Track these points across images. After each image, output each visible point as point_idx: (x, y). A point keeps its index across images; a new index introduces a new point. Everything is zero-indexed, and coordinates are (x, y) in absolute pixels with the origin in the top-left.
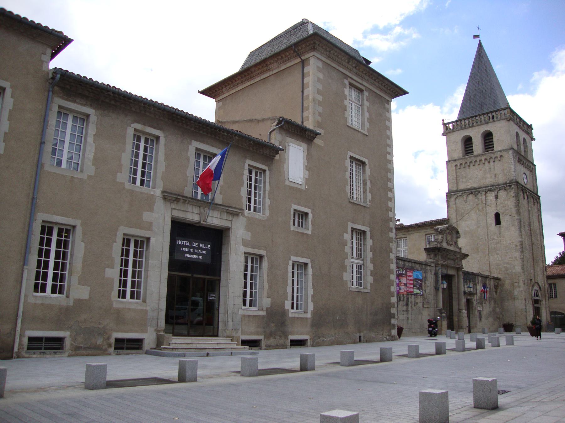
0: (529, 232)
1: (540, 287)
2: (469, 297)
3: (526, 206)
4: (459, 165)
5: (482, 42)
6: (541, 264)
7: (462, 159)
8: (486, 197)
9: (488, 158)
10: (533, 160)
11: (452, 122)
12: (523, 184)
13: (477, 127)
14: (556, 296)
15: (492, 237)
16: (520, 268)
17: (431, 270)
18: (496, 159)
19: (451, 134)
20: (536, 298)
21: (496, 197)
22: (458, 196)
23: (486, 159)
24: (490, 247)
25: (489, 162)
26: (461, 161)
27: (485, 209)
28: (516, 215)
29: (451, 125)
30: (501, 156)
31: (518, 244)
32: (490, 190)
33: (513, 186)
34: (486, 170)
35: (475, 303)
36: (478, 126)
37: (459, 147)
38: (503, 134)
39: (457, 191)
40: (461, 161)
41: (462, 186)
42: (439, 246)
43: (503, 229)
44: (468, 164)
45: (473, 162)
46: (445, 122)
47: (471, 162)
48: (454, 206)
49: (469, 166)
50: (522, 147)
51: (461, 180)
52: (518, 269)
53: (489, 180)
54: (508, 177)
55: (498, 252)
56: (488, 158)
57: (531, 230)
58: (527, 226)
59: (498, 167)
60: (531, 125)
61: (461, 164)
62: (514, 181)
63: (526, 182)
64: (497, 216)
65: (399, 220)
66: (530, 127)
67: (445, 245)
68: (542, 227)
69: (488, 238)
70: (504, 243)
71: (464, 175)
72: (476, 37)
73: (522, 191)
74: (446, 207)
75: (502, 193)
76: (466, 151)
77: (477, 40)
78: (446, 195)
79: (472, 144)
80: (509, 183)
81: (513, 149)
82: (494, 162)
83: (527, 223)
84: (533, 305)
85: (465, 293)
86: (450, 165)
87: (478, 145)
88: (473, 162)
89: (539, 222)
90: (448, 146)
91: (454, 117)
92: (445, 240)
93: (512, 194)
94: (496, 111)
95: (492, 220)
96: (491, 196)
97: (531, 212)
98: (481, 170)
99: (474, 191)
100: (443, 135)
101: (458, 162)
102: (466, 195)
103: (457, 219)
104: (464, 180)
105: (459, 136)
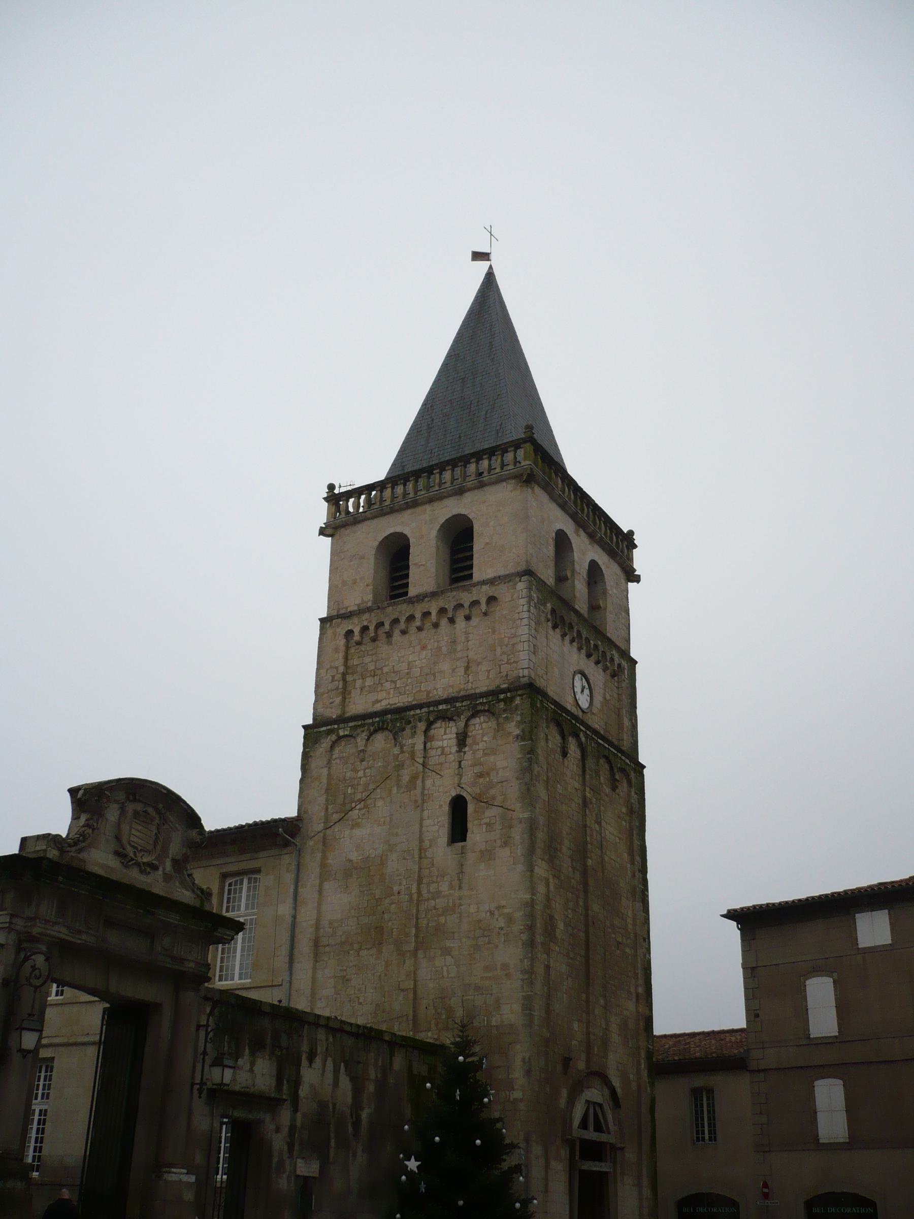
0: (578, 876)
1: (613, 1093)
4: (357, 630)
5: (496, 272)
8: (428, 739)
9: (450, 606)
10: (628, 641)
13: (427, 507)
14: (713, 1138)
15: (433, 888)
16: (517, 1007)
18: (475, 611)
19: (348, 531)
20: (591, 1135)
21: (462, 740)
22: (340, 738)
23: (442, 611)
24: (423, 923)
25: (452, 621)
27: (419, 783)
28: (517, 806)
30: (492, 600)
31: (518, 915)
32: (445, 717)
33: (518, 701)
34: (439, 649)
35: (278, 1142)
36: (430, 501)
37: (367, 572)
38: (509, 527)
39: (342, 720)
40: (370, 620)
41: (359, 704)
43: (471, 857)
44: (387, 626)
45: (403, 619)
47: (396, 621)
48: (325, 771)
49: (389, 635)
51: (359, 683)
52: (511, 1013)
53: (447, 682)
54: (505, 668)
55: (448, 944)
56: (450, 606)
57: (585, 873)
58: (566, 849)
59: (473, 635)
60: (631, 533)
62: (524, 681)
64: (458, 806)
66: (627, 541)
69: (419, 893)
70: (472, 909)
71: (371, 667)
72: (478, 256)
73: (559, 725)
74: (299, 775)
75: (481, 727)
76: (393, 588)
77: (482, 267)
78: (302, 732)
80: (503, 691)
81: (529, 572)
82: (468, 618)
86: (330, 631)
87: (425, 567)
88: (403, 619)
89: (631, 853)
90: (334, 569)
93: (513, 728)
94: (491, 452)
96: (445, 736)
98: (424, 648)
99: (391, 721)
100: (322, 532)
101: (355, 620)
102: (364, 735)
103: (327, 820)
104: (369, 682)
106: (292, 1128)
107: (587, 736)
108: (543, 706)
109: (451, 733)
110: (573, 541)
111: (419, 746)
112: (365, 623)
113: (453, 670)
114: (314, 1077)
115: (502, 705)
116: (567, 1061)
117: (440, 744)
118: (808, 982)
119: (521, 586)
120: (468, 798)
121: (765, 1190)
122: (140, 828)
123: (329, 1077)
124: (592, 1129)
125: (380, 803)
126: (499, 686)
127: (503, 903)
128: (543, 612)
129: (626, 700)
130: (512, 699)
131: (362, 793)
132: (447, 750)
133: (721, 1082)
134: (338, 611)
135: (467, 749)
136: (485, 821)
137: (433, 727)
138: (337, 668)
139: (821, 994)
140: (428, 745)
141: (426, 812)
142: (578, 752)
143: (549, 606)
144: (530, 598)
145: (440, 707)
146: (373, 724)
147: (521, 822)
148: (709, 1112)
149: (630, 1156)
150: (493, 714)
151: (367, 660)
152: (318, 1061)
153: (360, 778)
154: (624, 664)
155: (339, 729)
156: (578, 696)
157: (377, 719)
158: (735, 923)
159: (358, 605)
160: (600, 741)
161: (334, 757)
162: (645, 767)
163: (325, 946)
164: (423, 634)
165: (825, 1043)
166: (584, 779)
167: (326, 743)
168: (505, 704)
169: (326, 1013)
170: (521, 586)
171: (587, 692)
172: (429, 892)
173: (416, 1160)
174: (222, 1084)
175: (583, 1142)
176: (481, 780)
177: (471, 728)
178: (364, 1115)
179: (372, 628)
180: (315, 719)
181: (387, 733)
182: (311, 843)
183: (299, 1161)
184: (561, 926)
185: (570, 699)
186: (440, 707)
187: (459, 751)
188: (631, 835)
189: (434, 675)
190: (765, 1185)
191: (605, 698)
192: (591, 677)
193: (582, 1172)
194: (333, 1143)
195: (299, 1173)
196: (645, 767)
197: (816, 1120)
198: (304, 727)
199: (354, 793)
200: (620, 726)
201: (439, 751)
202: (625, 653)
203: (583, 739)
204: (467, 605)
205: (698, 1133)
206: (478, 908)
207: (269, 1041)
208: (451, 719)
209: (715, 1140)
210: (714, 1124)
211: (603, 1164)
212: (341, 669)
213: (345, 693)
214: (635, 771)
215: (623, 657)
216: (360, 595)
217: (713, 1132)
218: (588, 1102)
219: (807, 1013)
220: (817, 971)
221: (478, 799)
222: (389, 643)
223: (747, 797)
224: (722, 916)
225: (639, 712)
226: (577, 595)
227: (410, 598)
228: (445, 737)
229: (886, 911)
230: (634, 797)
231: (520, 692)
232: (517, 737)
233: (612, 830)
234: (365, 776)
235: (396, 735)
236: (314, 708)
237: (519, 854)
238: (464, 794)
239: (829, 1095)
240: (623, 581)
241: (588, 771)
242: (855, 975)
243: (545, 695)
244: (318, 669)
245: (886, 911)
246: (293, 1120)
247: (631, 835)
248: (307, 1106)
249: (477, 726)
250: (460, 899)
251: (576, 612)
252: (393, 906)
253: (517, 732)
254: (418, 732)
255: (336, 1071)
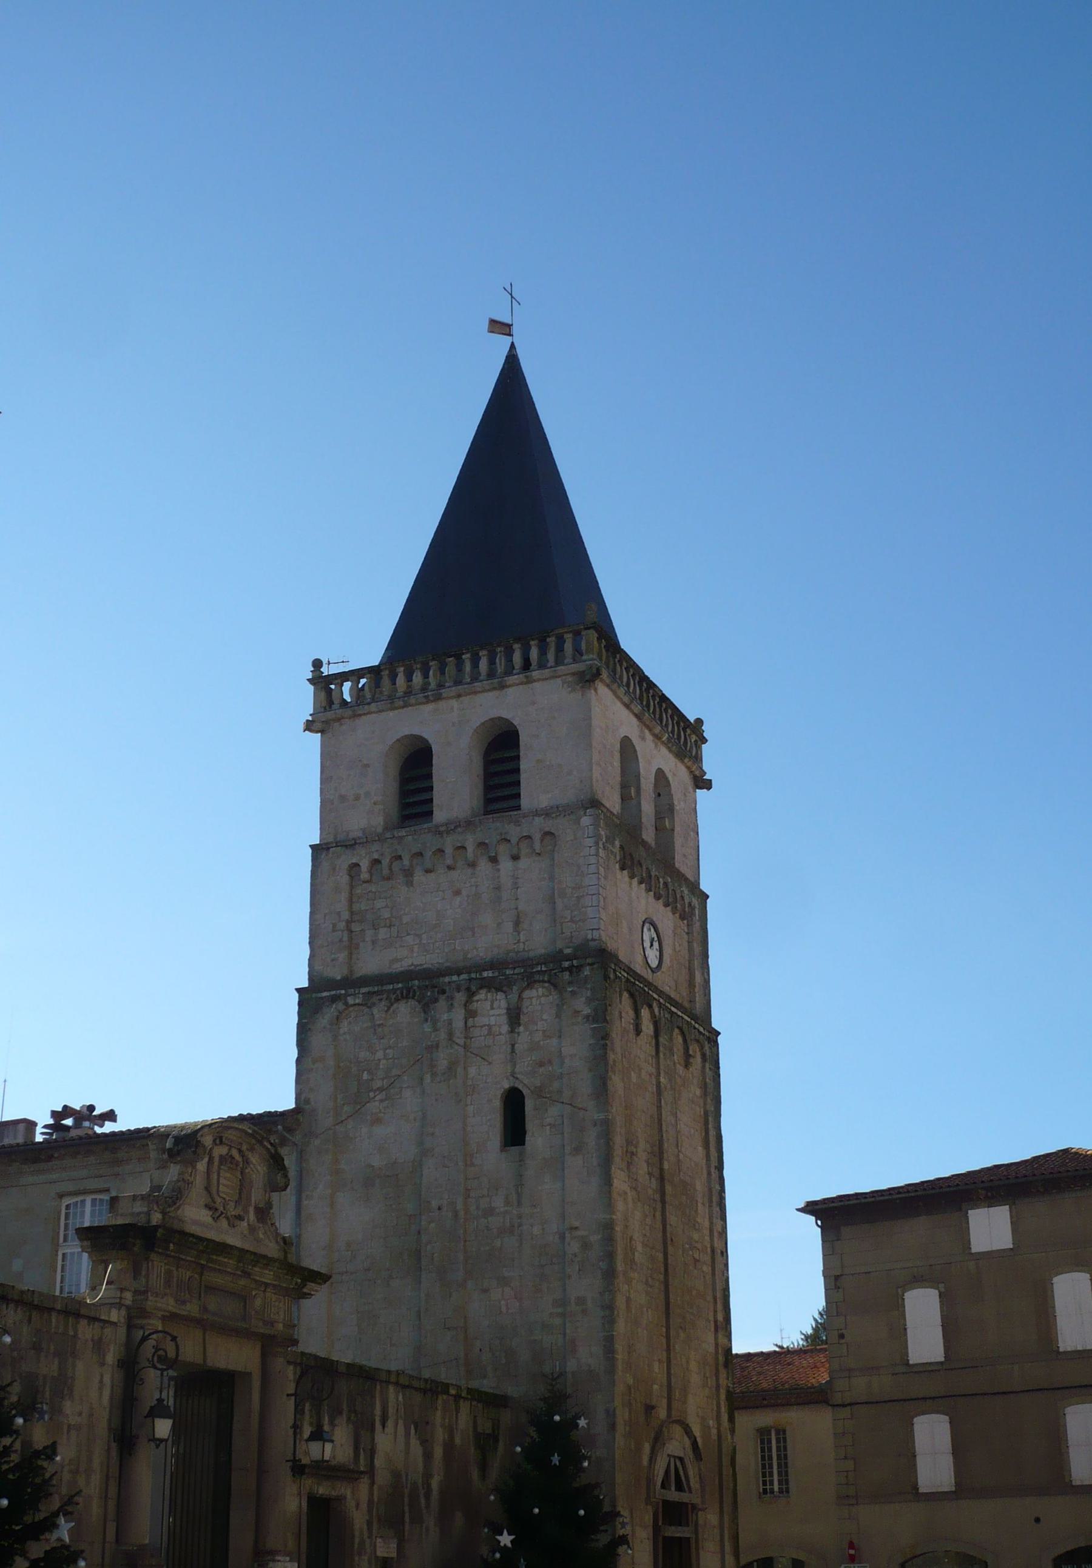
0: (654, 1184)
1: (694, 1443)
2: (322, 1490)
3: (648, 1068)
4: (365, 864)
6: (710, 1337)
7: (380, 839)
11: (354, 675)
12: (639, 968)
14: (785, 1491)
17: (99, 1346)
20: (673, 1495)
21: (514, 1017)
25: (494, 860)
26: (376, 847)
29: (347, 686)
31: (595, 1238)
33: (587, 971)
35: (359, 1519)
37: (378, 788)
38: (567, 733)
39: (350, 983)
41: (371, 963)
42: (156, 1218)
46: (325, 671)
49: (408, 874)
50: (648, 808)
51: (369, 933)
53: (490, 940)
57: (662, 1179)
58: (642, 1155)
60: (699, 722)
61: (377, 862)
63: (654, 963)
64: (514, 1104)
65: (111, 1116)
67: (194, 1216)
68: (720, 1167)
70: (536, 1230)
72: (500, 327)
74: (294, 1053)
75: (538, 1001)
77: (502, 344)
79: (430, 776)
80: (568, 958)
81: (594, 803)
82: (515, 858)
83: (642, 1150)
84: (656, 1530)
85: (298, 1469)
86: (325, 865)
87: (455, 787)
89: (706, 1146)
90: (326, 779)
91: (368, 648)
92: (196, 1193)
93: (582, 1005)
95: (486, 1122)
96: (492, 1009)
97: (667, 1096)
98: (458, 893)
99: (422, 987)
100: (309, 726)
104: (383, 933)
105: (384, 730)
106: (370, 1502)
107: (660, 1005)
108: (616, 977)
109: (499, 1007)
110: (637, 748)
111: (458, 1024)
112: (376, 856)
113: (499, 924)
114: (390, 1443)
115: (566, 976)
116: (649, 1409)
117: (485, 1021)
118: (907, 1295)
119: (586, 821)
120: (525, 1091)
121: (852, 1552)
122: (228, 1175)
123: (401, 1439)
124: (673, 1488)
125: (407, 1093)
126: (561, 951)
127: (577, 1224)
128: (612, 852)
129: (697, 948)
130: (579, 968)
131: (383, 1079)
132: (495, 1029)
133: (793, 1418)
134: (335, 837)
135: (521, 1029)
136: (548, 1120)
137: (476, 998)
138: (339, 913)
139: (923, 1309)
140: (470, 1022)
141: (471, 1109)
142: (651, 1027)
143: (617, 843)
144: (597, 837)
145: (485, 974)
146: (394, 991)
147: (595, 1125)
148: (779, 1456)
149: (710, 1517)
150: (555, 986)
151: (379, 903)
152: (390, 1423)
153: (379, 1060)
154: (695, 902)
155: (346, 995)
156: (648, 952)
157: (400, 985)
158: (813, 1218)
159: (364, 830)
160: (673, 1009)
161: (342, 1031)
162: (719, 1033)
163: (342, 1274)
164: (455, 874)
165: (927, 1369)
166: (658, 1063)
167: (330, 1012)
168: (571, 973)
169: (347, 1359)
170: (586, 821)
171: (656, 945)
172: (478, 1208)
173: (501, 1534)
174: (323, 1461)
175: (666, 1503)
176: (541, 1070)
177: (526, 1003)
178: (435, 1483)
179: (385, 862)
180: (311, 979)
181: (412, 1003)
182: (317, 1142)
183: (379, 1540)
184: (640, 1248)
185: (639, 959)
186: (485, 974)
187: (512, 1031)
188: (706, 1123)
189: (473, 930)
190: (851, 1545)
191: (674, 950)
192: (660, 926)
193: (665, 1538)
194: (407, 1519)
195: (379, 1554)
196: (719, 1033)
197: (915, 1465)
198: (298, 990)
199: (372, 1079)
200: (691, 984)
201: (485, 1031)
202: (694, 887)
203: (656, 1010)
204: (514, 840)
205: (764, 1483)
206: (543, 1229)
207: (345, 1406)
208: (499, 989)
209: (788, 1492)
210: (786, 1472)
211: (685, 1528)
212: (346, 915)
213: (352, 947)
214: (709, 1040)
215: (693, 894)
216: (363, 819)
217: (784, 1481)
218: (668, 1455)
219: (906, 1334)
220: (918, 1280)
221: (539, 1092)
222: (410, 883)
223: (845, 1068)
224: (798, 1210)
225: (711, 961)
226: (644, 820)
227: (437, 826)
228: (492, 1012)
229: (1007, 1207)
230: (709, 1073)
231: (589, 960)
232: (587, 1017)
233: (687, 1122)
234: (385, 1057)
235: (426, 1007)
236: (310, 965)
237: (595, 1164)
238: (520, 1087)
239: (932, 1437)
240: (691, 789)
241: (661, 1049)
242: (965, 1286)
243: (618, 962)
244: (312, 914)
245: (1007, 1207)
246: (371, 1493)
247: (706, 1123)
248: (382, 1477)
249: (534, 1000)
250: (520, 1217)
251: (644, 843)
252: (433, 1225)
253: (587, 1011)
254: (456, 1004)
255: (407, 1434)
